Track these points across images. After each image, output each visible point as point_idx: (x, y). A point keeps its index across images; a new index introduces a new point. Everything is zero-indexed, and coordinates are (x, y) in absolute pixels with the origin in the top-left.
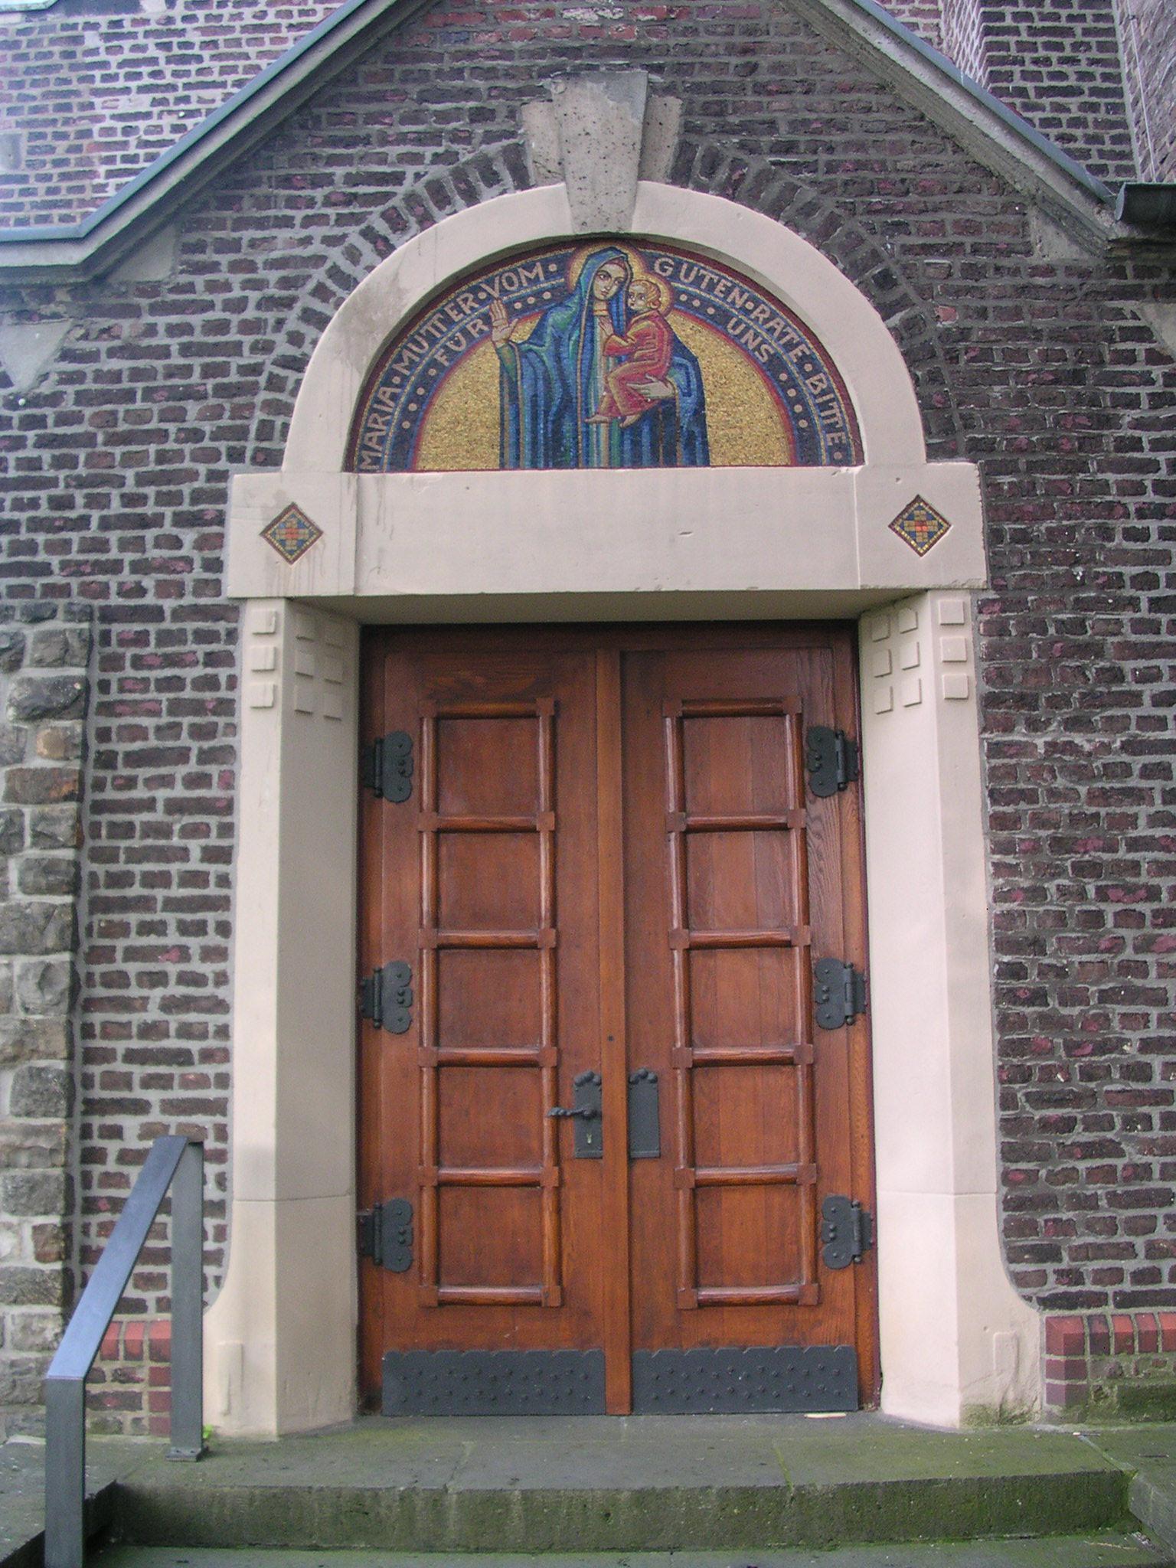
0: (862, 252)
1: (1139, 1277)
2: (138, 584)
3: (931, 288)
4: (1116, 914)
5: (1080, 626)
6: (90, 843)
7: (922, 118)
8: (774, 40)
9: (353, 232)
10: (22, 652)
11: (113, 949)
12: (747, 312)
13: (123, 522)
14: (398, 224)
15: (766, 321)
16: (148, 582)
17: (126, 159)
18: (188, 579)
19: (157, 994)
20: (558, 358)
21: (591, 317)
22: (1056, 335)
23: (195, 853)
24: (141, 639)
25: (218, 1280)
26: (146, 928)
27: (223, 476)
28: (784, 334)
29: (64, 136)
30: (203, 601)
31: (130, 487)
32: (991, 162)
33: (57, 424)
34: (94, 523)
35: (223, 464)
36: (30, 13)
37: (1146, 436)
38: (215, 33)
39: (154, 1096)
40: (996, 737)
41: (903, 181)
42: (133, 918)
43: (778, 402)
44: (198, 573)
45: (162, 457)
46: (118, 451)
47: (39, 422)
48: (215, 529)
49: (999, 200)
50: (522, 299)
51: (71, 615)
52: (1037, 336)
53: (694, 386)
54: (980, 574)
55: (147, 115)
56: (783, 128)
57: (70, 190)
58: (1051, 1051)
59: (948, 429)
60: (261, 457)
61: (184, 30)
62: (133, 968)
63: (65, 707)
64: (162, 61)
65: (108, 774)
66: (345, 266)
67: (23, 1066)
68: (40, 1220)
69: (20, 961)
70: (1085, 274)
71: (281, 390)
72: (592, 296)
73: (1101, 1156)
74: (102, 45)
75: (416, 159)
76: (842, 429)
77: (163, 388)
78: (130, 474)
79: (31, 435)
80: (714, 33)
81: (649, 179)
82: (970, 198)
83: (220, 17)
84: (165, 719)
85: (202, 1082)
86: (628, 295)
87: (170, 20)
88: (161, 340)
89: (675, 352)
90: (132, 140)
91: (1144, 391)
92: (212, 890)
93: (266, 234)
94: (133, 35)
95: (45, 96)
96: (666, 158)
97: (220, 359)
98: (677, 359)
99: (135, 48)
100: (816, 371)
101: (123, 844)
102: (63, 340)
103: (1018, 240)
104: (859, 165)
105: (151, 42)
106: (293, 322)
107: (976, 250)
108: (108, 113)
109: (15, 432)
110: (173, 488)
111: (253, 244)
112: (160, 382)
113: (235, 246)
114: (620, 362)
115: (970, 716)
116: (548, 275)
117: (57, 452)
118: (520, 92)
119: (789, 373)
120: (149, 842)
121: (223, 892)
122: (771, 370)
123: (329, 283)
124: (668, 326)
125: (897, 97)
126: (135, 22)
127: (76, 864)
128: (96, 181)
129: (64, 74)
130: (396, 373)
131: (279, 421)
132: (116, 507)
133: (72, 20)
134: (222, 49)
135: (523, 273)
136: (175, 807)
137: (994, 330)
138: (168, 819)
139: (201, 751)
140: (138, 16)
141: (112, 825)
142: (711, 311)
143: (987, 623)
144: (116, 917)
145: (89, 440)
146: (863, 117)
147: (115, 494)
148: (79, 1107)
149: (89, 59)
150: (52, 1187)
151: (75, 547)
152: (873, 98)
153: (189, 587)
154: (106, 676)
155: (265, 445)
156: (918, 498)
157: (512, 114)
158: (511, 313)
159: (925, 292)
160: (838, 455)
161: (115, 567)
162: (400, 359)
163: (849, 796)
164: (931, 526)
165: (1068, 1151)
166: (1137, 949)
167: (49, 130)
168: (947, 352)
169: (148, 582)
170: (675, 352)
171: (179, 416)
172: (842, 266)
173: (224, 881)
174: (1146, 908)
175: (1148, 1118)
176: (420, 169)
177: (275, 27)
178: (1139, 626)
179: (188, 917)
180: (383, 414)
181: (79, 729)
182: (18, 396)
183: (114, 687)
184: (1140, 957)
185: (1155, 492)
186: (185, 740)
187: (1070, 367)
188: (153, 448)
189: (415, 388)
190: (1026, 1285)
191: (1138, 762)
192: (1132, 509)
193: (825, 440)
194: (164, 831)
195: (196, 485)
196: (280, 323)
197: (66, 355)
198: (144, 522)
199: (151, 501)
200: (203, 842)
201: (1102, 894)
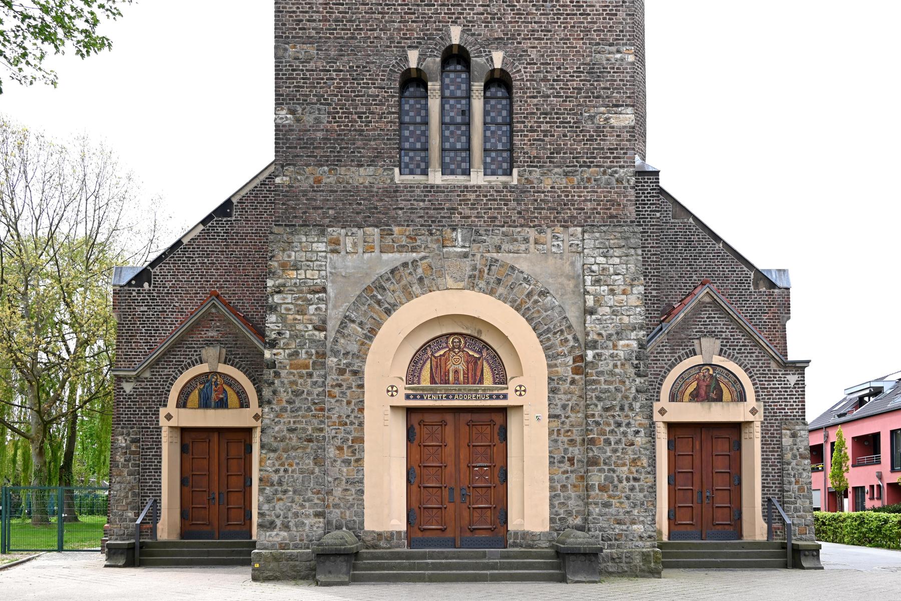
13: (144, 414)
14: (183, 369)
24: (147, 432)
36: (121, 286)
47: (131, 398)
75: (186, 358)
87: (150, 290)
96: (223, 359)
113: (159, 372)
122: (237, 393)
136: (153, 455)
145: (138, 402)
161: (143, 421)
177: (171, 293)
194: (152, 459)
197: (134, 388)
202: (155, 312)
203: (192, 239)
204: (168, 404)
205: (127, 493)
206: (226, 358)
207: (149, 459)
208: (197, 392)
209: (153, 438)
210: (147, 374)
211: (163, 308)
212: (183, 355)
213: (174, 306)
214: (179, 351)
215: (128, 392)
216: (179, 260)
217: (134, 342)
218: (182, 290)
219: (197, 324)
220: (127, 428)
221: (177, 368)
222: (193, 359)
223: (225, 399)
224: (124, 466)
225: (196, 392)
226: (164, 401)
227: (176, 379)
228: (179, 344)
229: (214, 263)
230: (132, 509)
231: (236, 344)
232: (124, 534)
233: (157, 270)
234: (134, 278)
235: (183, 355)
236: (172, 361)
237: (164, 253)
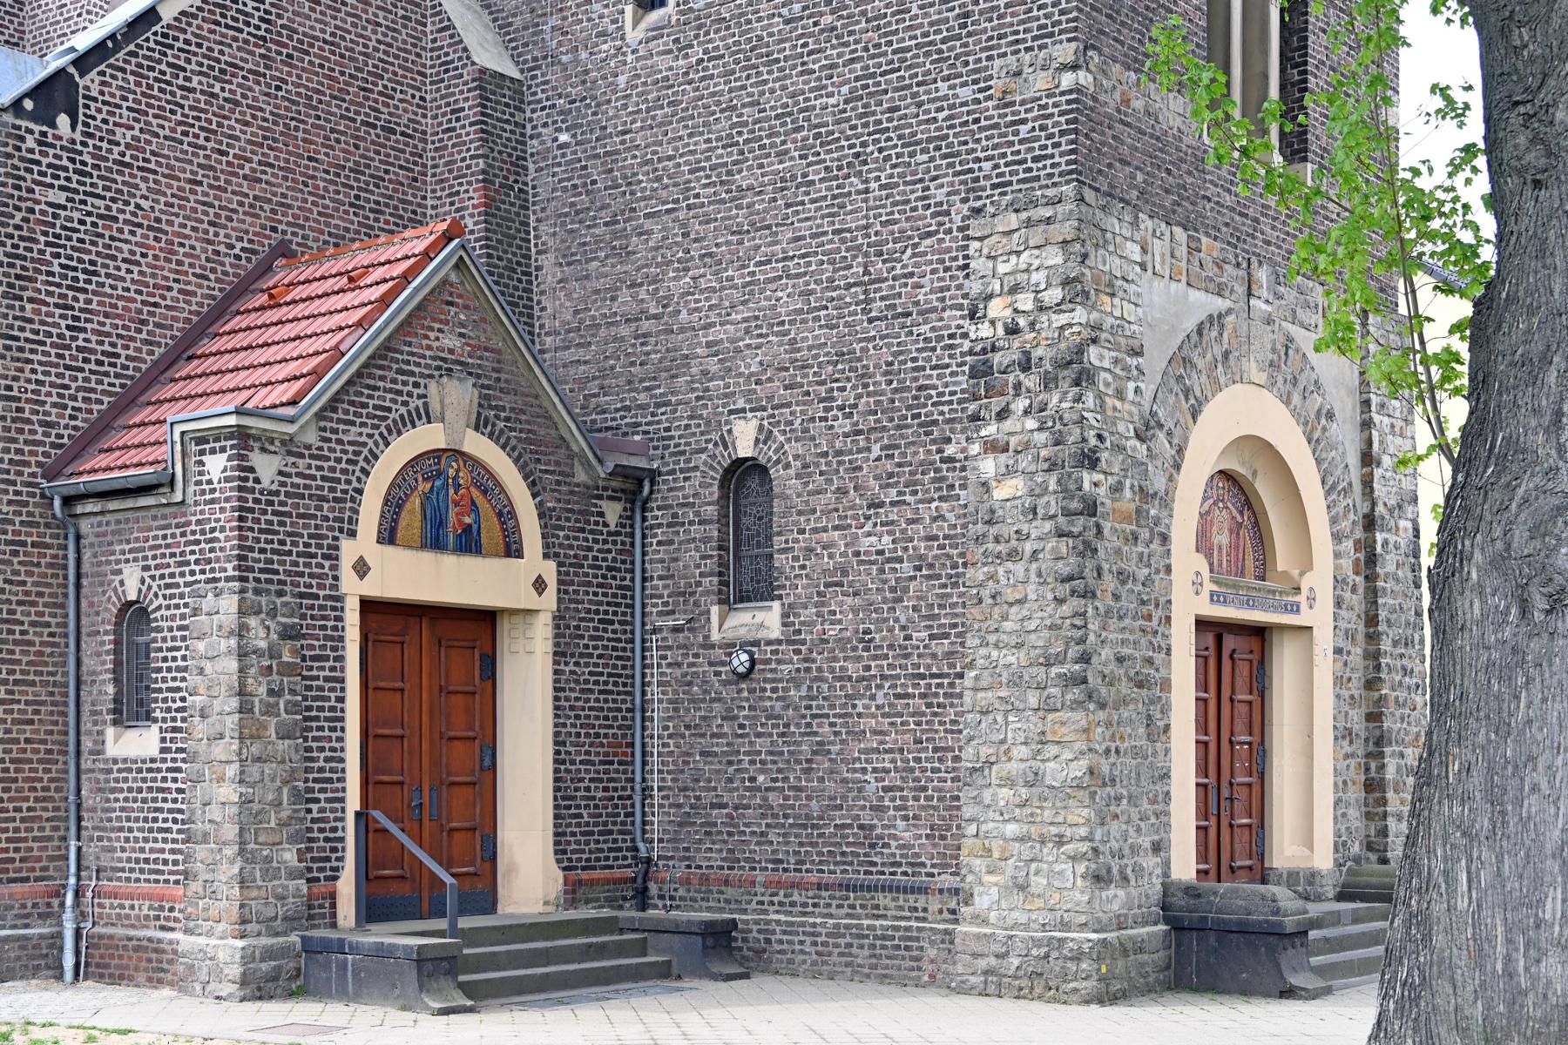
24: (312, 607)
32: (567, 436)
35: (337, 534)
39: (322, 796)
54: (554, 607)
62: (314, 745)
69: (287, 742)
85: (337, 790)
88: (313, 472)
122: (500, 515)
132: (301, 548)
133: (18, 122)
173: (342, 710)
197: (280, 473)
202: (89, 214)
203: (183, 13)
204: (360, 529)
208: (418, 501)
210: (312, 437)
211: (108, 208)
213: (138, 206)
215: (266, 483)
217: (31, 300)
223: (475, 527)
224: (270, 710)
230: (292, 839)
231: (498, 380)
233: (89, 82)
234: (32, 93)
237: (112, 36)
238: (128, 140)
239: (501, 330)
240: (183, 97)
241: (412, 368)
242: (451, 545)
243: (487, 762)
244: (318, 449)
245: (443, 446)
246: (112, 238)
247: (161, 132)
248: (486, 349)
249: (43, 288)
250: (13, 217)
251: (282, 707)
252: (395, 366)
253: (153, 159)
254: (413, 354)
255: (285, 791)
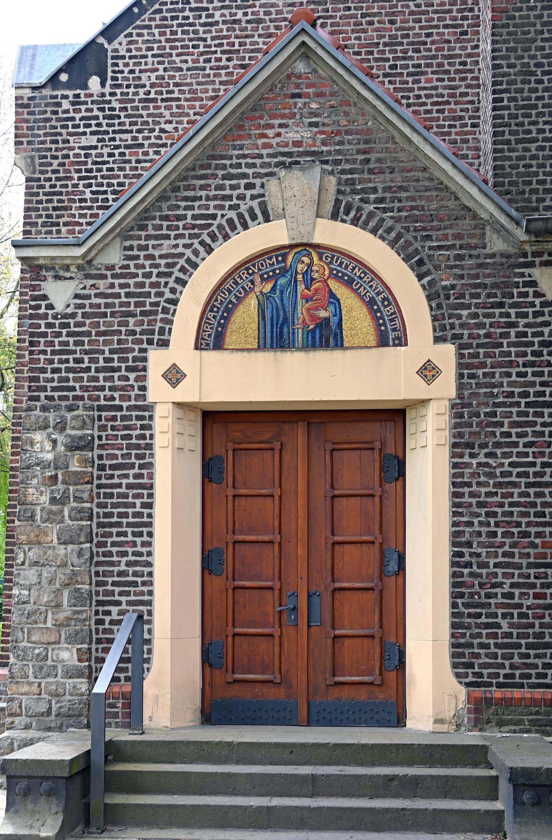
0: (411, 249)
1: (506, 676)
2: (112, 396)
3: (440, 266)
4: (502, 533)
5: (494, 414)
6: (96, 501)
7: (442, 183)
8: (378, 146)
9: (197, 246)
10: (66, 423)
11: (107, 542)
12: (361, 278)
15: (369, 282)
16: (116, 395)
17: (87, 171)
18: (133, 394)
19: (124, 559)
20: (282, 300)
21: (296, 282)
22: (495, 285)
23: (138, 505)
24: (114, 418)
25: (148, 669)
26: (119, 534)
27: (145, 351)
28: (376, 288)
29: (56, 157)
30: (139, 403)
31: (107, 355)
33: (75, 327)
34: (93, 370)
35: (145, 346)
36: (35, 88)
37: (530, 331)
38: (126, 103)
39: (123, 599)
40: (456, 460)
41: (431, 215)
42: (114, 530)
43: (372, 318)
44: (137, 391)
45: (119, 342)
46: (101, 339)
47: (68, 325)
48: (143, 373)
49: (473, 222)
50: (267, 273)
51: (86, 409)
52: (485, 286)
53: (338, 312)
54: (453, 393)
55: (96, 147)
56: (380, 191)
57: (61, 186)
58: (473, 586)
59: (443, 328)
60: (160, 343)
61: (110, 101)
62: (114, 550)
63: (85, 446)
64: (101, 118)
65: (103, 473)
66: (193, 258)
67: (72, 588)
68: (80, 646)
69: (70, 547)
70: (509, 256)
71: (168, 313)
72: (296, 271)
73: (492, 628)
74: (71, 108)
75: (222, 207)
76: (399, 330)
77: (119, 312)
78: (107, 349)
79: (64, 331)
80: (351, 144)
81: (321, 217)
82: (460, 222)
83: (127, 94)
84: (125, 451)
85: (142, 593)
86: (312, 271)
87: (103, 95)
88: (117, 290)
89: (330, 297)
90: (89, 161)
91: (530, 310)
92: (145, 519)
93: (159, 242)
94: (86, 103)
95: (45, 135)
96: (329, 207)
97: (142, 299)
98: (331, 300)
99: (87, 110)
100: (389, 304)
101: (110, 501)
102: (76, 289)
103: (481, 241)
104: (412, 208)
105: (95, 107)
106: (172, 284)
107: (461, 247)
108: (77, 145)
109: (57, 330)
110: (125, 355)
111: (154, 247)
112: (117, 309)
113: (146, 248)
114: (307, 301)
115: (446, 452)
116: (278, 262)
117: (76, 339)
118: (267, 175)
119: (378, 306)
120: (120, 500)
121: (150, 520)
122: (370, 304)
123: (186, 266)
124: (328, 285)
125: (431, 174)
126: (87, 96)
127: (91, 509)
128: (73, 182)
129: (53, 123)
130: (215, 306)
131: (167, 327)
132: (101, 363)
134: (130, 112)
135: (267, 261)
136: (130, 486)
137: (466, 285)
138: (127, 491)
139: (140, 464)
140: (88, 92)
141: (105, 493)
142: (346, 278)
143: (455, 413)
144: (107, 530)
145: (89, 334)
146: (415, 184)
147: (101, 357)
148: (94, 603)
149: (65, 116)
150: (85, 633)
151: (85, 380)
152: (420, 174)
153: (133, 397)
154: (101, 433)
155: (162, 337)
156: (429, 361)
157: (263, 186)
158: (263, 279)
159: (437, 268)
160: (397, 342)
161: (102, 389)
162: (216, 300)
163: (399, 483)
164: (434, 372)
165: (478, 626)
166: (510, 547)
167: (49, 154)
168: (445, 295)
169: (116, 395)
170: (330, 297)
171: (126, 324)
172: (402, 256)
173: (150, 516)
174: (515, 530)
175: (512, 614)
176: (224, 212)
177: (154, 100)
178: (519, 414)
179: (136, 530)
180: (210, 324)
181: (90, 455)
182: (57, 314)
183: (104, 438)
184: (512, 550)
185: (532, 356)
186: (133, 460)
187: (498, 300)
188: (116, 338)
189: (223, 313)
190: (460, 677)
191: (515, 471)
192: (521, 363)
193: (392, 335)
194: (126, 496)
195: (134, 354)
196: (166, 283)
197: (77, 296)
198: (113, 370)
199: (116, 361)
200: (141, 500)
201: (497, 524)
202: (117, 147)
204: (173, 339)
205: (58, 592)
206: (338, 202)
207: (120, 495)
209: (129, 437)
211: (135, 138)
212: (215, 198)
213: (162, 131)
214: (202, 188)
215: (59, 307)
216: (173, 18)
217: (66, 224)
218: (182, 92)
219: (254, 109)
220: (57, 408)
221: (197, 236)
222: (243, 208)
223: (334, 321)
225: (252, 302)
226: (162, 331)
227: (195, 266)
228: (202, 167)
229: (260, 21)
230: (72, 639)
231: (368, 161)
232: (49, 712)
235: (215, 198)
236: (185, 217)
238: (153, 80)
239: (367, 108)
240: (205, 32)
241: (244, 170)
242: (461, 361)
243: (393, 566)
244: (123, 267)
245: (286, 242)
246: (138, 161)
247: (184, 66)
248: (347, 133)
249: (77, 213)
250: (51, 164)
251: (66, 513)
252: (220, 173)
253: (176, 89)
254: (245, 156)
255: (66, 593)
